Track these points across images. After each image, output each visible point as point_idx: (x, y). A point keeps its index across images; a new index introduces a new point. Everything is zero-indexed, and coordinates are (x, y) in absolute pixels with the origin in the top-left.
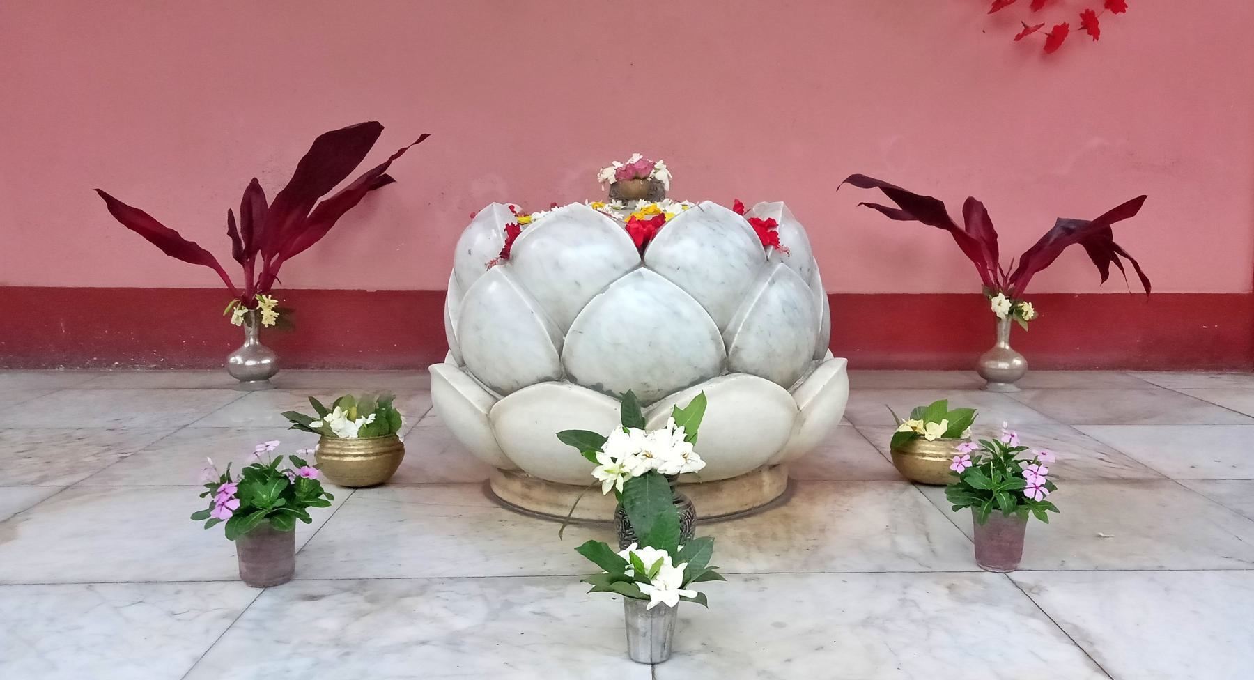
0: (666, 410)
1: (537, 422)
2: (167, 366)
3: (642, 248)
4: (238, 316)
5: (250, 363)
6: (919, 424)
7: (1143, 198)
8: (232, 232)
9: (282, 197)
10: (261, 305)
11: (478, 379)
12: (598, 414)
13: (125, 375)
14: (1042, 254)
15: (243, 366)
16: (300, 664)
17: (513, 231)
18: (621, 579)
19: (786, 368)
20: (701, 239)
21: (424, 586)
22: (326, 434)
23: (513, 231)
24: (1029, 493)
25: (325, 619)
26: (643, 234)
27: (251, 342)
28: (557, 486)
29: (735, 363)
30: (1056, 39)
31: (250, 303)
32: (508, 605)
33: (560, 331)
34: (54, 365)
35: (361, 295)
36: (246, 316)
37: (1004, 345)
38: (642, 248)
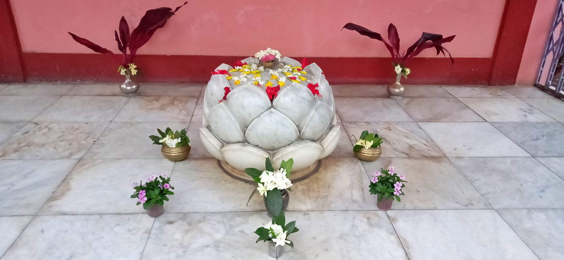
2: (96, 82)
3: (272, 100)
4: (123, 72)
5: (129, 88)
6: (363, 141)
7: (454, 36)
8: (117, 39)
9: (137, 31)
10: (130, 67)
11: (216, 136)
13: (83, 86)
15: (126, 89)
16: (173, 256)
17: (227, 90)
20: (293, 97)
22: (164, 145)
23: (227, 90)
24: (395, 193)
25: (175, 233)
26: (272, 93)
29: (302, 137)
31: (127, 67)
32: (231, 227)
33: (245, 128)
34: (57, 81)
35: (165, 57)
36: (125, 72)
37: (398, 83)
38: (272, 100)
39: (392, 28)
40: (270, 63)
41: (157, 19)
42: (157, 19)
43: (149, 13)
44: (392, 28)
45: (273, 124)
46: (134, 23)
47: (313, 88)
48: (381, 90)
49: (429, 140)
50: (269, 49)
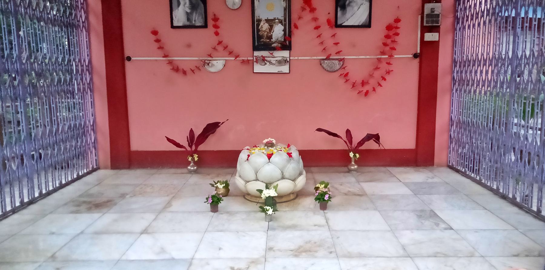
0: (273, 186)
1: (253, 187)
2: (171, 167)
4: (190, 159)
5: (192, 168)
8: (188, 141)
9: (200, 135)
11: (243, 179)
12: (262, 186)
14: (361, 143)
17: (249, 156)
18: (264, 211)
19: (293, 178)
20: (280, 157)
21: (237, 213)
22: (217, 188)
23: (249, 156)
26: (269, 156)
27: (192, 164)
28: (256, 197)
30: (367, 93)
31: (192, 156)
33: (256, 173)
39: (348, 132)
40: (270, 145)
41: (211, 128)
42: (211, 128)
43: (209, 125)
44: (348, 132)
45: (270, 170)
46: (198, 132)
47: (290, 155)
48: (345, 169)
49: (362, 189)
50: (270, 139)
